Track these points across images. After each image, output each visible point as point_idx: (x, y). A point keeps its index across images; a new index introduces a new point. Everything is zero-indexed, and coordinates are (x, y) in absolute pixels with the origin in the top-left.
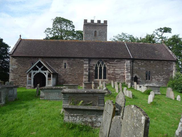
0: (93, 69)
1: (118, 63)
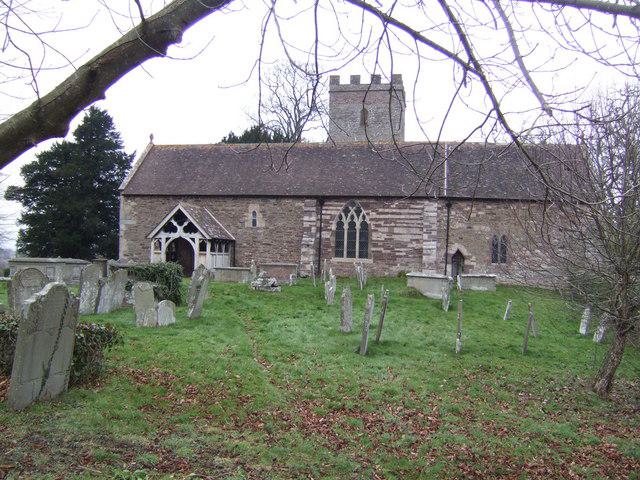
1: (402, 211)
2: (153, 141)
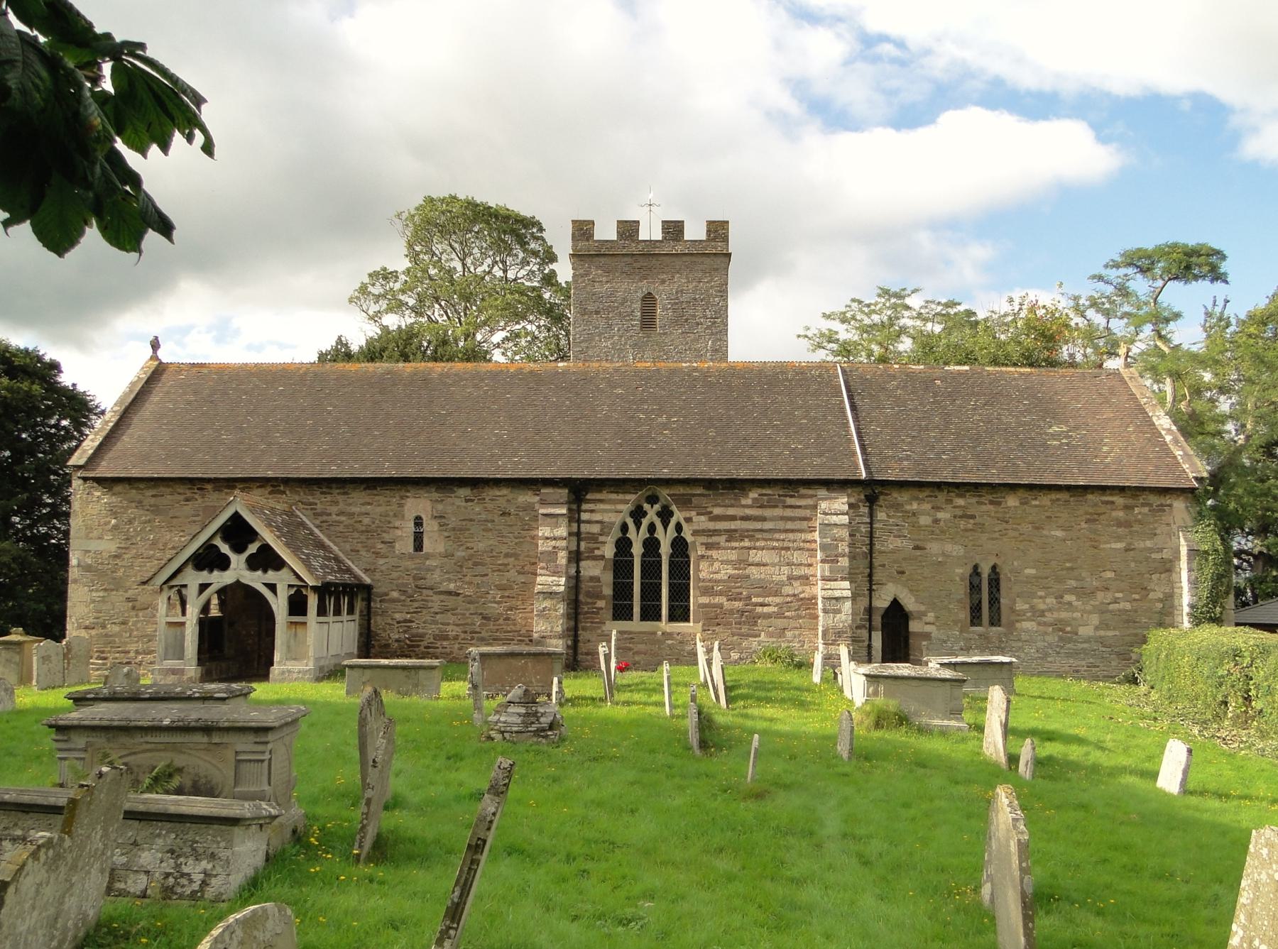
0: (602, 557)
1: (768, 513)
2: (160, 353)
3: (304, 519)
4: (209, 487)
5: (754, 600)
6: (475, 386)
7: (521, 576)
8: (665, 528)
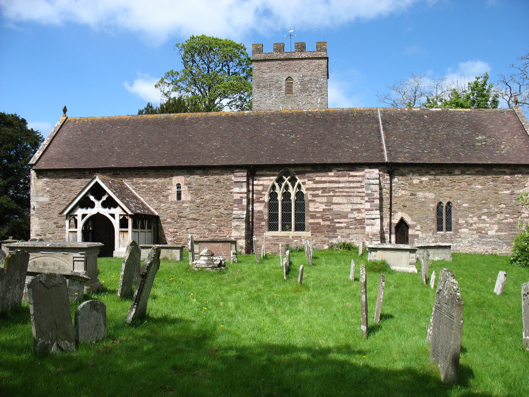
0: (264, 201)
3: (128, 186)
4: (87, 172)
5: (335, 220)
6: (206, 123)
7: (226, 211)
8: (293, 187)
